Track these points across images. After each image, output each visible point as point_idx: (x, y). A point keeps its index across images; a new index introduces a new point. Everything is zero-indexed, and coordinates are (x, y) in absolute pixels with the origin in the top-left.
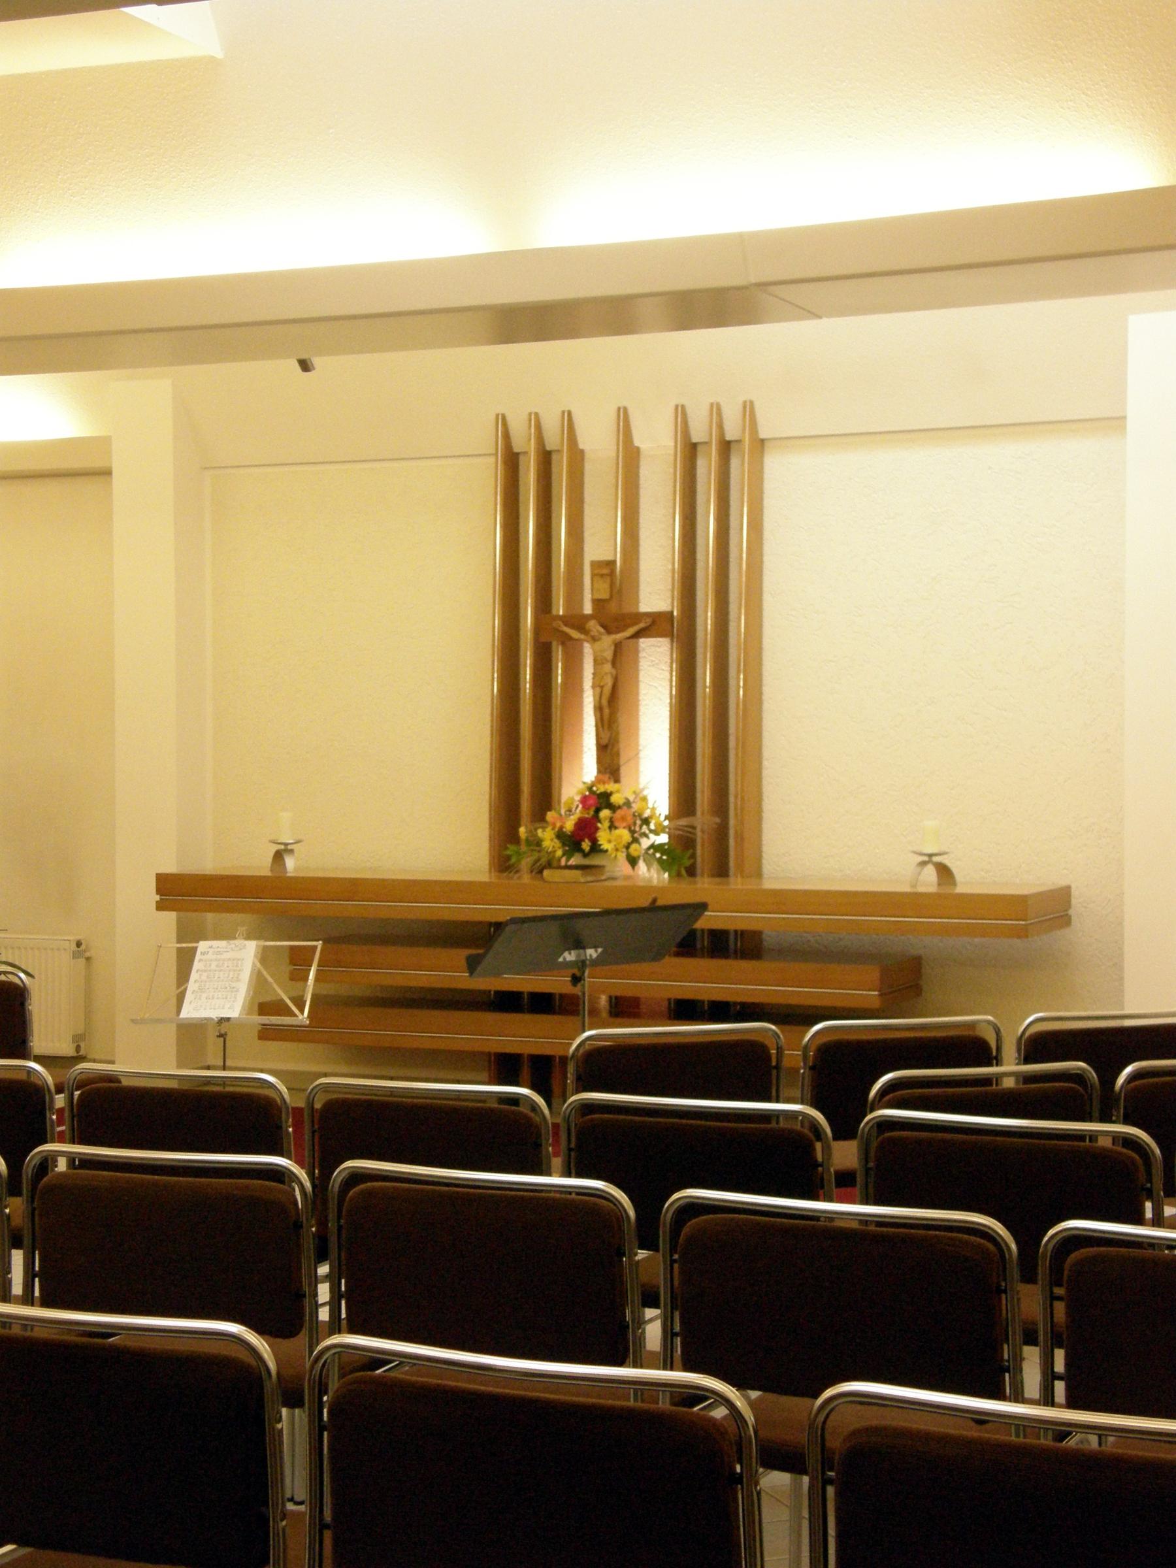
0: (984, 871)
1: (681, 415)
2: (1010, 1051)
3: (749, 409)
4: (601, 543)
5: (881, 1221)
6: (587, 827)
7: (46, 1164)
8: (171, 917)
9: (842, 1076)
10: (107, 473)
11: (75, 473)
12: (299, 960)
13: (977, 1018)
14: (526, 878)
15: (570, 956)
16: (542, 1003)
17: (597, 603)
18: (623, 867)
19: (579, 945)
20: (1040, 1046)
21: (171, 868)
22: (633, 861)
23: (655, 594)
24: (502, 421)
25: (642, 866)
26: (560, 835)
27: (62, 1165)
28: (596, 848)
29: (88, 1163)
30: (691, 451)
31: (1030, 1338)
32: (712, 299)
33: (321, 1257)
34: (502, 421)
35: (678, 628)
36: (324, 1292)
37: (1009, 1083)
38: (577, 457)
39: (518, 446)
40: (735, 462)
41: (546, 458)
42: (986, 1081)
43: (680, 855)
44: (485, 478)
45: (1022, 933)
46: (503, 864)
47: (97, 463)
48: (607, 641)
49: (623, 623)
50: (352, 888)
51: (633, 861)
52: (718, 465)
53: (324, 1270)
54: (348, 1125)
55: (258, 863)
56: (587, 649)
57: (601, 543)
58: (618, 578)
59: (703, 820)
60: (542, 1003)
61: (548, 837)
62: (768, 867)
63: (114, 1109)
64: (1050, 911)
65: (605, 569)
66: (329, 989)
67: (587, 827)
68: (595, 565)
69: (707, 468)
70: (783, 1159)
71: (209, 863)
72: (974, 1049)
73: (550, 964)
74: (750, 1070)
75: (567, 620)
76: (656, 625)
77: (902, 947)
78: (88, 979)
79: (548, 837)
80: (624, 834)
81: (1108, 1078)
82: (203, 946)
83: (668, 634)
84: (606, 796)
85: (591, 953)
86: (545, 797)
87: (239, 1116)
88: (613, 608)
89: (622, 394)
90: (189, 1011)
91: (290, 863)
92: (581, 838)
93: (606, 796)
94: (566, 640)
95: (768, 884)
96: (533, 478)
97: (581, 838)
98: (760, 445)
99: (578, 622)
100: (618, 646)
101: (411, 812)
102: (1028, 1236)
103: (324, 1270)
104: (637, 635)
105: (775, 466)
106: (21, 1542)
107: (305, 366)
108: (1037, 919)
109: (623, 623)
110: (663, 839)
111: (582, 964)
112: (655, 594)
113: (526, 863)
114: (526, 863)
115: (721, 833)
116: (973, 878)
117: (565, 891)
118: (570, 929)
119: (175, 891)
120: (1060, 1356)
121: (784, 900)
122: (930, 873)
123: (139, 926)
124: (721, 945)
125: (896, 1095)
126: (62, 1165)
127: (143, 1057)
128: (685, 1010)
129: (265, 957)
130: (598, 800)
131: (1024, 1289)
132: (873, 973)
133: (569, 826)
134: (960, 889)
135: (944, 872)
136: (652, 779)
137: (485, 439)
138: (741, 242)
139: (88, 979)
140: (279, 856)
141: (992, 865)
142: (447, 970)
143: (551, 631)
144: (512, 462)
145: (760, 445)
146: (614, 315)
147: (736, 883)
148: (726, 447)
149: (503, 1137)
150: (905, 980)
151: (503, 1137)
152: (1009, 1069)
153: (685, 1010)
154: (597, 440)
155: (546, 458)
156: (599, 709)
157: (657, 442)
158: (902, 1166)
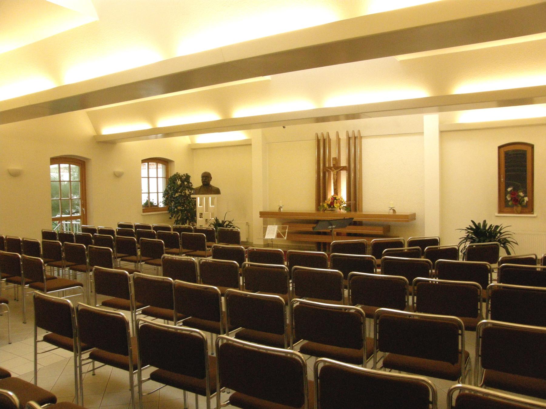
0: (400, 211)
1: (347, 132)
2: (406, 244)
3: (359, 131)
4: (334, 155)
5: (385, 278)
6: (332, 203)
7: (245, 264)
8: (262, 219)
9: (377, 249)
10: (251, 145)
11: (246, 145)
12: (284, 228)
13: (401, 238)
14: (322, 212)
15: (330, 227)
16: (325, 234)
17: (333, 165)
18: (339, 210)
19: (332, 225)
20: (412, 243)
21: (262, 210)
22: (340, 209)
23: (343, 163)
24: (317, 134)
25: (342, 210)
26: (328, 205)
27: (247, 265)
28: (334, 207)
29: (251, 265)
30: (349, 138)
31: (411, 295)
32: (353, 114)
33: (290, 279)
34: (317, 134)
35: (347, 169)
36: (291, 285)
37: (406, 251)
38: (330, 140)
39: (319, 138)
40: (357, 140)
41: (324, 140)
42: (402, 250)
43: (348, 208)
44: (314, 144)
45: (408, 221)
46: (318, 209)
47: (249, 143)
48: (335, 171)
49: (338, 168)
50: (292, 214)
51: (340, 209)
52: (354, 141)
53: (291, 281)
54: (294, 259)
55: (276, 209)
56: (332, 173)
57: (334, 155)
58: (337, 160)
59: (352, 202)
60: (325, 234)
61: (325, 205)
62: (363, 210)
63: (257, 255)
64: (413, 217)
65: (335, 159)
66: (290, 231)
67: (332, 203)
68: (333, 158)
69: (352, 141)
70: (368, 266)
71: (268, 210)
72: (400, 244)
73: (327, 229)
74: (361, 248)
75: (328, 168)
76: (344, 168)
77: (387, 225)
78: (249, 229)
79: (325, 205)
80: (338, 204)
81: (423, 249)
82: (268, 226)
83: (346, 170)
84: (335, 198)
85: (334, 226)
86: (325, 198)
87: (276, 257)
88: (336, 166)
89: (337, 130)
90: (266, 237)
91: (282, 209)
92: (331, 205)
93: (335, 198)
94: (328, 171)
95: (364, 213)
96: (322, 144)
97: (331, 205)
98: (361, 137)
99: (331, 168)
100: (337, 172)
101: (300, 199)
102: (411, 280)
103: (291, 281)
104: (341, 170)
105: (364, 141)
106: (243, 327)
107: (284, 127)
108: (410, 219)
109: (338, 168)
110: (345, 205)
111: (332, 228)
112: (343, 163)
113: (322, 210)
114: (322, 210)
115: (355, 204)
116: (399, 212)
117: (328, 216)
118: (330, 222)
119: (263, 214)
120: (415, 297)
121: (367, 216)
122: (392, 211)
123: (258, 221)
124: (355, 223)
125: (388, 253)
126: (247, 265)
127: (257, 243)
128: (349, 235)
129: (279, 228)
130: (334, 199)
131: (410, 286)
132: (382, 228)
133: (329, 203)
134: (397, 214)
135: (394, 211)
136: (343, 195)
137: (314, 137)
138: (358, 106)
139: (249, 229)
140: (280, 209)
141: (403, 209)
142: (309, 228)
143: (325, 171)
144: (318, 141)
145: (361, 137)
146: (336, 118)
147: (358, 213)
148: (355, 138)
149: (320, 262)
150: (387, 229)
151: (320, 262)
152: (406, 248)
153: (349, 235)
154: (333, 137)
155: (324, 140)
156: (334, 183)
157: (343, 137)
158: (388, 267)
